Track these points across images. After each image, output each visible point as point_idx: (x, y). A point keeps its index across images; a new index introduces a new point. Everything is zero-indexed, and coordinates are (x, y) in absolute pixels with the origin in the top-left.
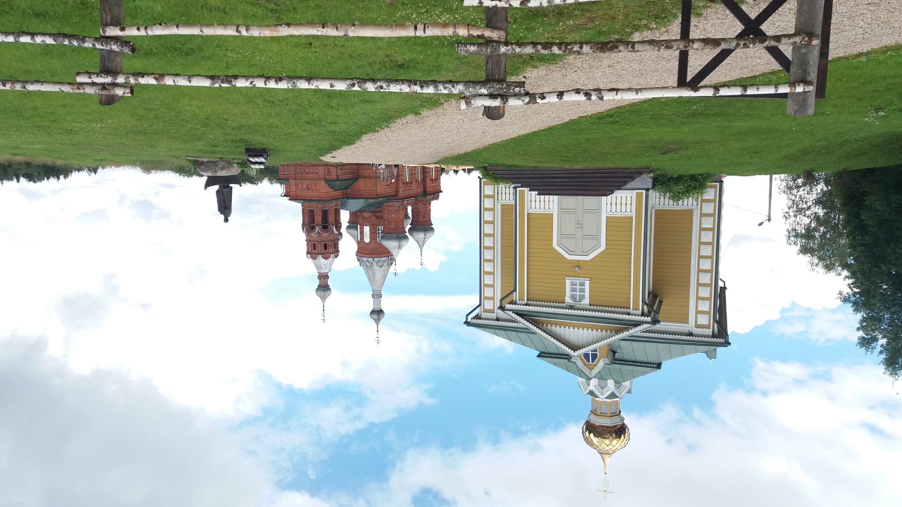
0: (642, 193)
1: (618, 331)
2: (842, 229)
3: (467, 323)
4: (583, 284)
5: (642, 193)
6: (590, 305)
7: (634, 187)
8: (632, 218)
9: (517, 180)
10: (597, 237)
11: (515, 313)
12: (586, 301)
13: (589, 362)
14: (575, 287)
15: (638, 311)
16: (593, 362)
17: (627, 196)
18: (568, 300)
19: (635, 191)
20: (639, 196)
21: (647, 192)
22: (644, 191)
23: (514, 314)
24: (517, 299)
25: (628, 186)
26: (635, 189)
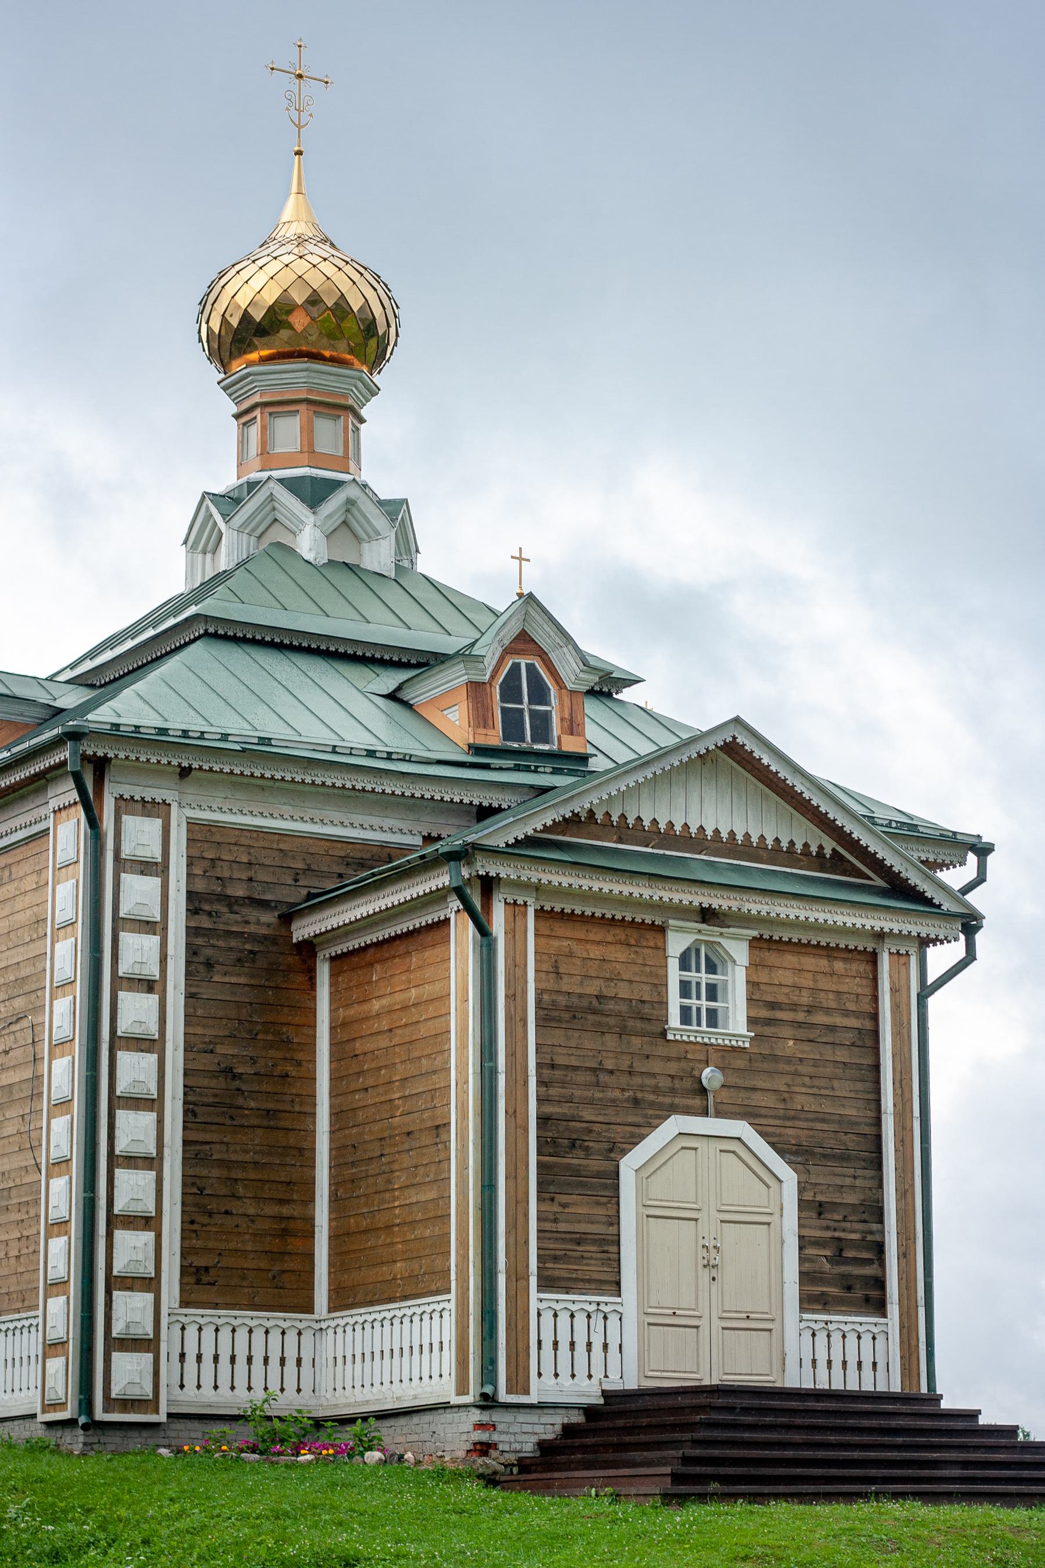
0: (509, 1391)
1: (572, 823)
2: (419, 1554)
3: (983, 850)
4: (686, 1014)
5: (509, 1391)
6: (662, 930)
7: (532, 1417)
8: (542, 1287)
9: (1028, 1457)
10: (650, 1214)
11: (929, 902)
12: (677, 943)
13: (530, 668)
14: (694, 995)
15: (510, 900)
16: (516, 667)
17: (553, 1380)
18: (738, 951)
19: (533, 1399)
20: (519, 1382)
21: (488, 1389)
22: (503, 1397)
23: (936, 901)
24: (914, 961)
25: (559, 1420)
26: (531, 1406)
